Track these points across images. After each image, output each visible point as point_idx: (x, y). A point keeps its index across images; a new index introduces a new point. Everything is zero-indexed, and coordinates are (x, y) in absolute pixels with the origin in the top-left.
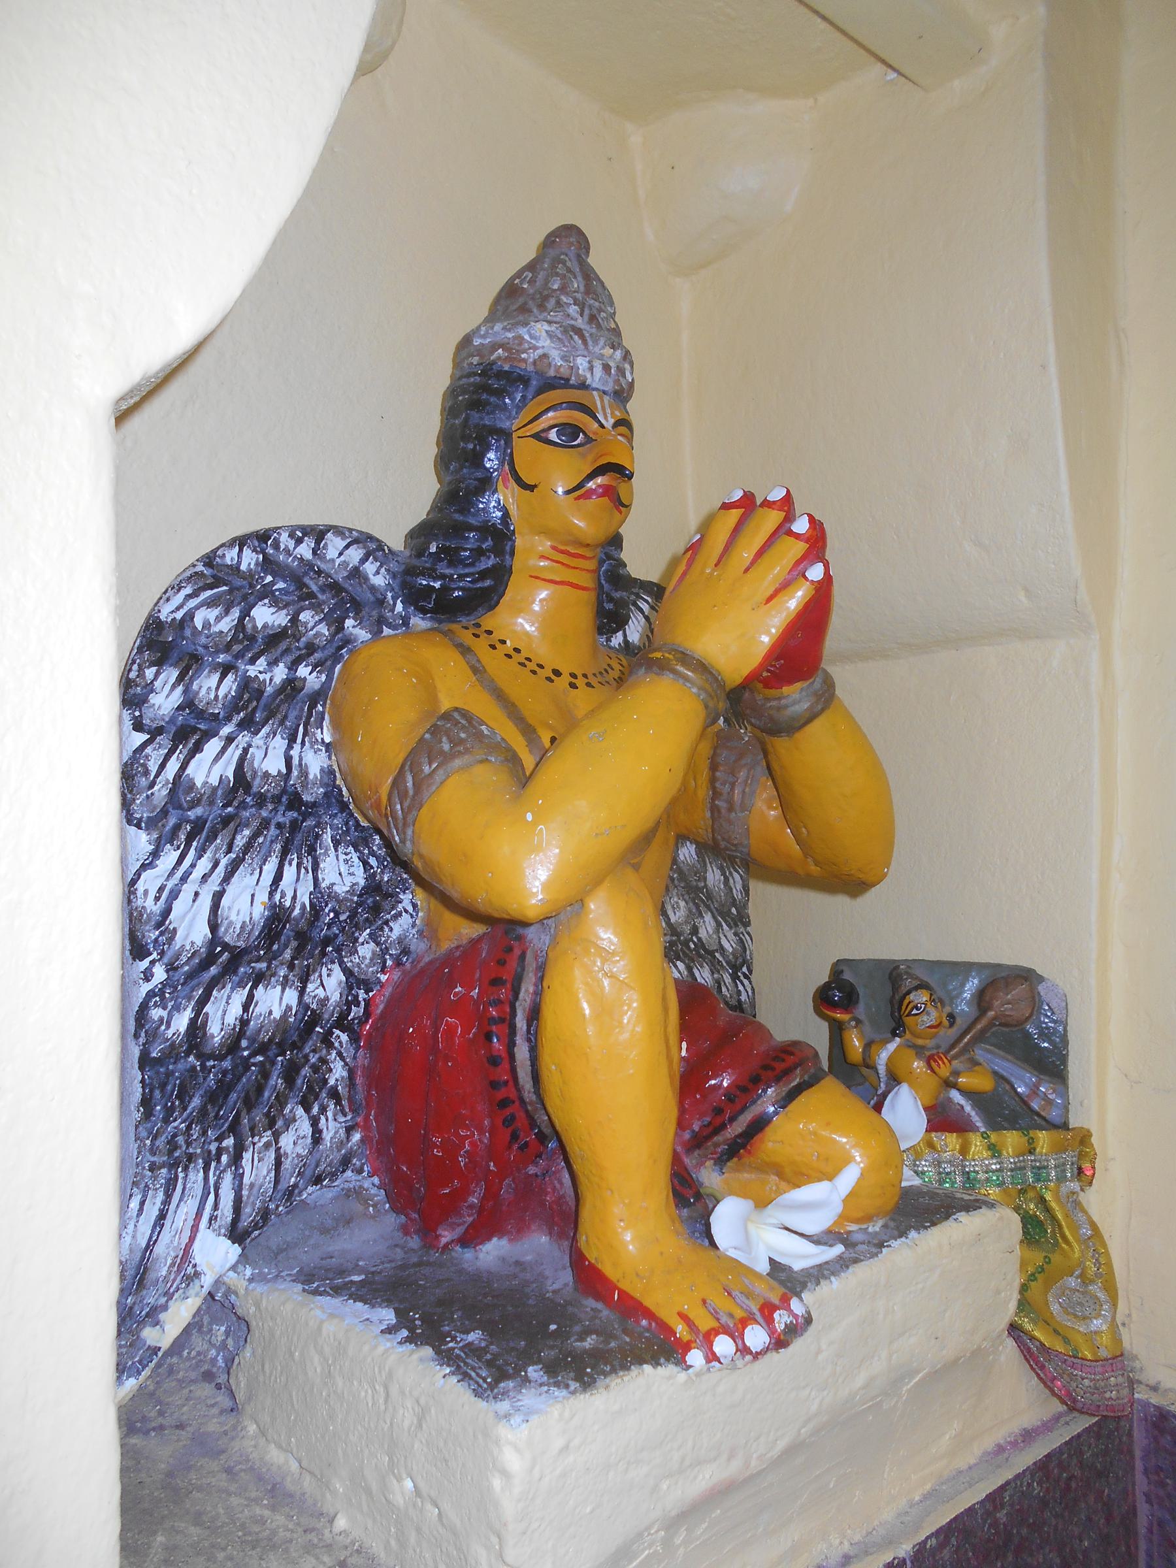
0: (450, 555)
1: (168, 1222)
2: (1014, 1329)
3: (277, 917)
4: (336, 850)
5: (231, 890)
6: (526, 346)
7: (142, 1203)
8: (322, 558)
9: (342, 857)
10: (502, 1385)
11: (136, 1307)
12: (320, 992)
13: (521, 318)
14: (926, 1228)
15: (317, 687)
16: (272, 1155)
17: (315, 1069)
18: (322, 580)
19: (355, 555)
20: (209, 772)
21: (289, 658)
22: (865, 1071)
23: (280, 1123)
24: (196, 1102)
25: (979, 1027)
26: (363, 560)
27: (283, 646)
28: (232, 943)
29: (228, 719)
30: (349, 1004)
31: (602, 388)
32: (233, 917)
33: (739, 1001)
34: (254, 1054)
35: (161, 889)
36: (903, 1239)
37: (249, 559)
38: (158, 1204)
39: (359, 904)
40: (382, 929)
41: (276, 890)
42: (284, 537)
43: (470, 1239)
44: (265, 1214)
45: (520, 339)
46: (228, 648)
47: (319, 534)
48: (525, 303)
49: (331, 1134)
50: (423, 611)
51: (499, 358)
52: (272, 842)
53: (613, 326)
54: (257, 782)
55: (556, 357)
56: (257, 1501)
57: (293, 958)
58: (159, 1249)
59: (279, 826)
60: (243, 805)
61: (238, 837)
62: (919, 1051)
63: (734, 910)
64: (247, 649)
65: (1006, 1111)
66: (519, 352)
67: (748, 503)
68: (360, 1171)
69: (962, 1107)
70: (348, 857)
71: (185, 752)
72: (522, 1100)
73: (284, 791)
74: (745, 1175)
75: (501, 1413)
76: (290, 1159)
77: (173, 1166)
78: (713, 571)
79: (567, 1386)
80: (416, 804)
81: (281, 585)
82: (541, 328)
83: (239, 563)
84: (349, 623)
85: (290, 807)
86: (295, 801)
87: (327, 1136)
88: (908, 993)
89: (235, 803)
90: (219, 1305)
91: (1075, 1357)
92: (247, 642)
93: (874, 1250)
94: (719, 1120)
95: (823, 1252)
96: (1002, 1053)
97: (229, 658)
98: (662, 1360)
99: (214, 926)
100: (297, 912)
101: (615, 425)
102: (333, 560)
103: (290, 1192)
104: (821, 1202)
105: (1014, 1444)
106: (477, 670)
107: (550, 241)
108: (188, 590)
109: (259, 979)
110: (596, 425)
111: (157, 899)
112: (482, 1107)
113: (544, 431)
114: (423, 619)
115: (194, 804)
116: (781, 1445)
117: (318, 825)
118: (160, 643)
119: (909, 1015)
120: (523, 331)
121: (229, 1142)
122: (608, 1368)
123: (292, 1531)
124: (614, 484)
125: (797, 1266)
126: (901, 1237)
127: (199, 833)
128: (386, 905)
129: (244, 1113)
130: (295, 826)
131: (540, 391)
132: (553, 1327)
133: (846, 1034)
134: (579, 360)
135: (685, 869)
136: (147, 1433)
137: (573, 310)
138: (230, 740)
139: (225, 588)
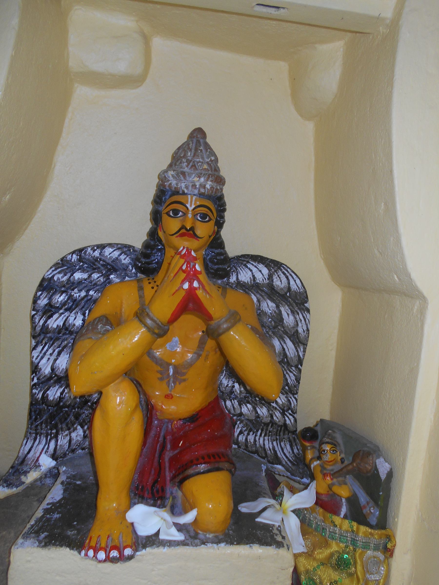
7: (27, 442)
16: (68, 438)
19: (116, 253)
21: (86, 289)
23: (72, 429)
28: (58, 374)
29: (61, 309)
35: (38, 356)
47: (102, 247)
54: (71, 327)
55: (174, 183)
58: (30, 456)
61: (63, 343)
63: (287, 388)
64: (72, 286)
71: (46, 317)
77: (36, 434)
81: (86, 265)
83: (71, 259)
92: (72, 285)
98: (75, 549)
99: (53, 369)
102: (107, 256)
107: (191, 136)
111: (36, 359)
115: (50, 332)
118: (46, 285)
121: (54, 431)
127: (53, 340)
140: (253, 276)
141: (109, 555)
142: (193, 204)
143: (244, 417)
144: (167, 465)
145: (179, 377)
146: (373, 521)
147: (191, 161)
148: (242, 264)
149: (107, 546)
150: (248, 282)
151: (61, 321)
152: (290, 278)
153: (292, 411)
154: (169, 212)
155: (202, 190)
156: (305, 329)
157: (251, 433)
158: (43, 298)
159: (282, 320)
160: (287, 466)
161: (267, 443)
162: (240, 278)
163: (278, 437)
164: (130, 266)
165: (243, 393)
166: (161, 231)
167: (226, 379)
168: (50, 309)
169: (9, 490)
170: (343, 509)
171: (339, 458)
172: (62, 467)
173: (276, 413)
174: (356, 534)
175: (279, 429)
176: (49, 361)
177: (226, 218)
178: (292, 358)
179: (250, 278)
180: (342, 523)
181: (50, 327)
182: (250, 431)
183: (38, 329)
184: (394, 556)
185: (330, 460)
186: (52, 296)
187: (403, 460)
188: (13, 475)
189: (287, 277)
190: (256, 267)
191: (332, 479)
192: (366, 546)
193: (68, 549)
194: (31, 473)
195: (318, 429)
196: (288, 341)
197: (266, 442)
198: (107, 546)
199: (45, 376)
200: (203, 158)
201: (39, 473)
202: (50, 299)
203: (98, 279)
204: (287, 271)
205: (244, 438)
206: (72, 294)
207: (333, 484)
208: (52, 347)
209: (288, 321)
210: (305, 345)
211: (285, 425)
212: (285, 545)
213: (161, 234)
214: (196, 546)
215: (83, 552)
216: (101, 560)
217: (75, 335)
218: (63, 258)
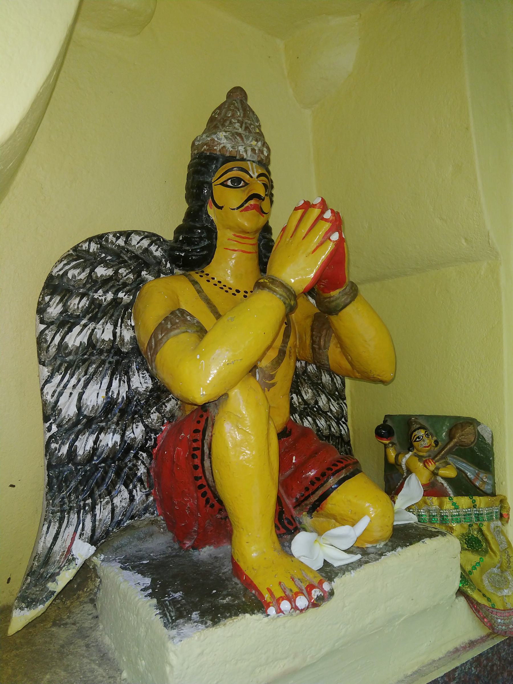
0: (188, 241)
1: (60, 537)
2: (460, 592)
3: (110, 404)
4: (138, 373)
5: (87, 392)
6: (216, 143)
7: (48, 528)
8: (130, 245)
9: (141, 375)
10: (178, 621)
11: (45, 574)
12: (132, 435)
13: (214, 131)
14: (407, 546)
15: (129, 301)
16: (110, 506)
17: (130, 469)
18: (129, 255)
19: (145, 243)
20: (75, 340)
22: (397, 467)
24: (73, 484)
25: (448, 447)
26: (150, 245)
27: (111, 284)
28: (88, 415)
29: (84, 317)
30: (146, 440)
31: (251, 159)
32: (89, 403)
33: (341, 434)
34: (100, 463)
35: (54, 392)
36: (393, 552)
37: (94, 247)
38: (56, 528)
39: (150, 396)
40: (162, 407)
41: (109, 391)
42: (111, 237)
43: (195, 547)
44: (107, 533)
45: (213, 140)
46: (84, 285)
47: (128, 234)
48: (217, 124)
49: (139, 497)
50: (178, 266)
51: (205, 150)
52: (106, 370)
53: (258, 131)
54: (99, 344)
55: (229, 146)
56: (94, 661)
57: (118, 421)
58: (56, 548)
59: (110, 363)
60: (92, 354)
61: (90, 368)
62: (420, 458)
63: (337, 393)
65: (463, 487)
66: (213, 146)
67: (307, 206)
68: (153, 514)
69: (443, 484)
70: (144, 375)
71: (63, 332)
72: (208, 485)
73: (112, 347)
74: (321, 519)
75: (171, 636)
76: (119, 508)
77: (62, 511)
78: (290, 240)
79: (206, 623)
80: (155, 352)
81: (109, 258)
82: (222, 135)
84: (144, 273)
85: (116, 354)
86: (118, 352)
87: (137, 498)
88: (415, 431)
89: (88, 354)
90: (87, 571)
91: (493, 608)
92: (95, 283)
93: (377, 557)
94: (307, 494)
95: (352, 557)
96: (461, 459)
97: (85, 290)
98: (256, 611)
100: (120, 400)
101: (259, 176)
102: (135, 246)
103: (119, 523)
104: (347, 534)
105: (464, 648)
106: (200, 291)
107: (229, 95)
108: (65, 262)
109: (101, 430)
110: (248, 176)
111: (52, 396)
112: (192, 488)
113: (225, 181)
114: (180, 270)
115: (70, 354)
116: (323, 652)
117: (129, 361)
118: (54, 286)
119: (415, 441)
120: (214, 137)
121: (89, 501)
122: (228, 615)
123: (104, 677)
124: (258, 203)
125: (336, 564)
126: (392, 550)
127: (71, 367)
128: (163, 396)
129: (96, 489)
130: (118, 363)
131: (223, 163)
132: (214, 591)
133: (388, 450)
134: (240, 148)
135: (311, 375)
136: (60, 626)
137: (237, 125)
138: (85, 326)
139: (82, 260)
142: (255, 172)
153: (345, 419)
158: (55, 304)
165: (301, 405)
171: (433, 441)
186: (67, 301)
188: (35, 586)
193: (247, 615)
194: (62, 573)
198: (301, 590)
199: (69, 420)
206: (96, 297)
217: (105, 354)
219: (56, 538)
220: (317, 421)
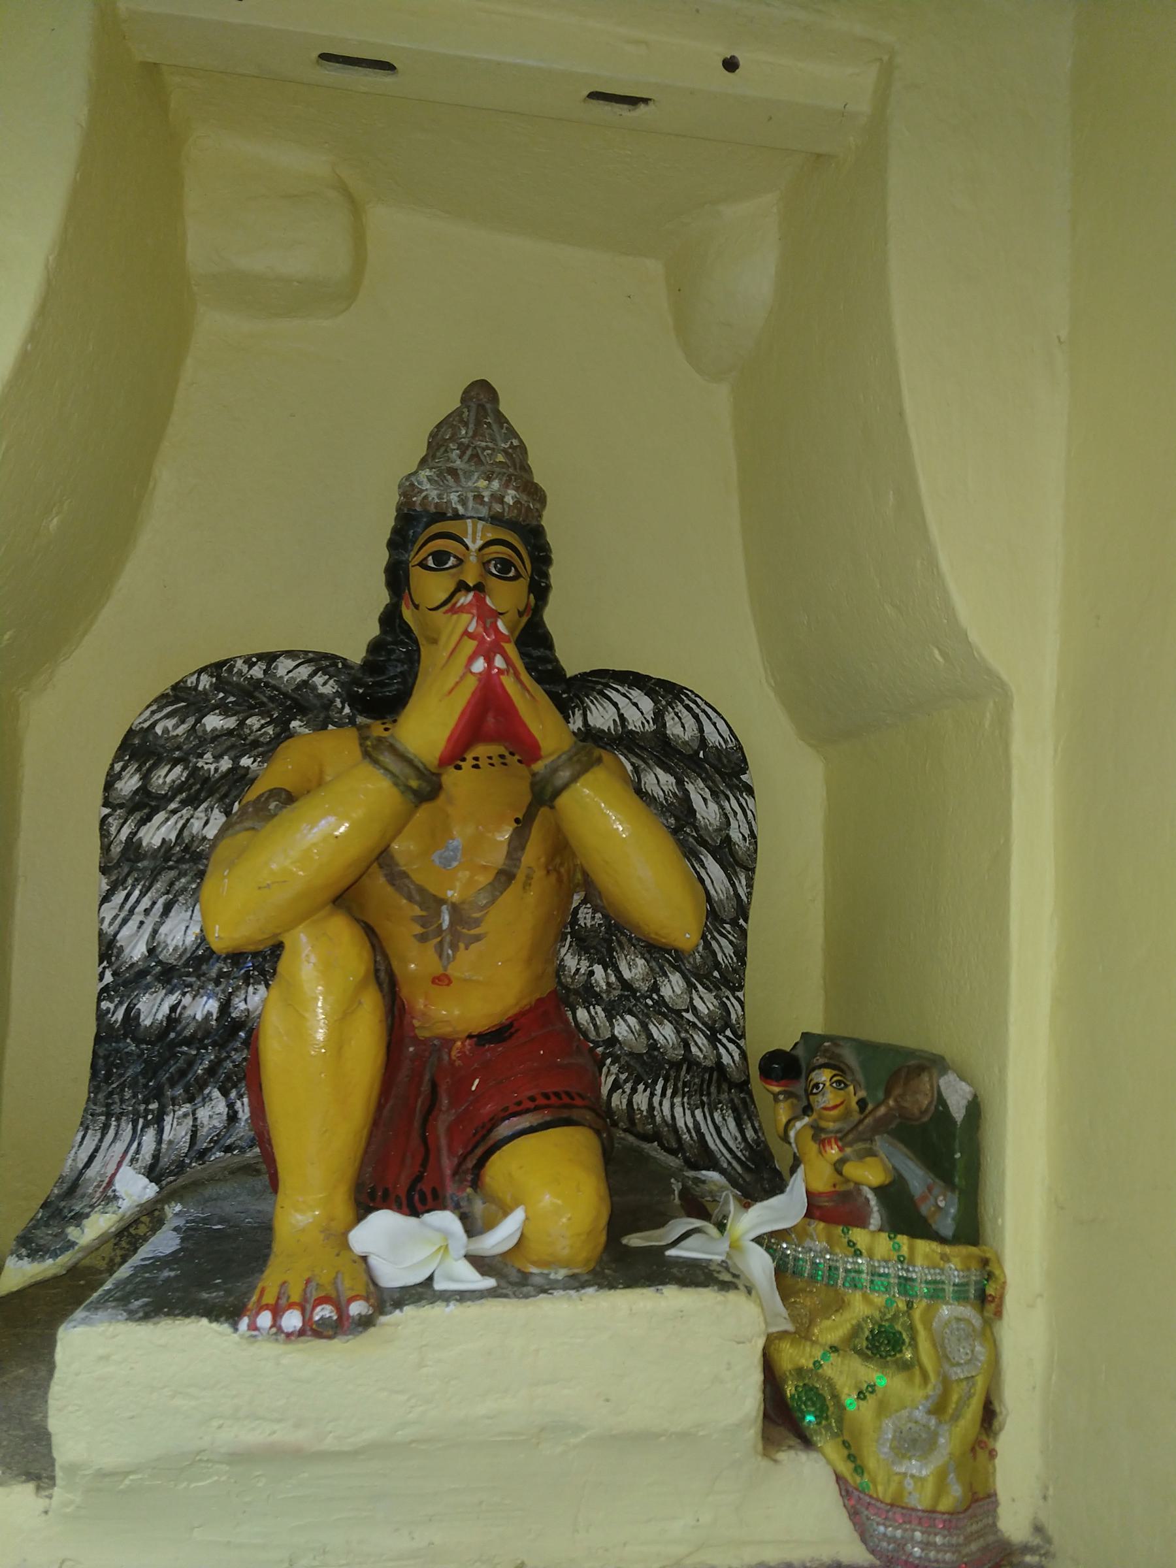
7: (83, 1138)
16: (189, 1121)
19: (304, 672)
23: (199, 1099)
29: (171, 800)
32: (169, 942)
47: (270, 658)
54: (195, 844)
55: (433, 494)
58: (90, 1173)
63: (716, 974)
77: (109, 1115)
81: (232, 699)
83: (197, 685)
99: (151, 951)
102: (281, 677)
107: (466, 397)
111: (111, 924)
118: (138, 748)
129: (166, 1087)
140: (621, 716)
141: (311, 1318)
143: (621, 1048)
144: (443, 1142)
145: (465, 931)
146: (947, 1226)
147: (468, 446)
148: (593, 689)
149: (305, 1300)
150: (609, 729)
151: (170, 831)
152: (703, 717)
154: (425, 559)
155: (498, 508)
156: (747, 833)
157: (641, 1087)
159: (692, 812)
160: (733, 1172)
161: (682, 1115)
162: (591, 722)
163: (705, 1098)
164: (338, 700)
166: (408, 608)
167: (573, 954)
168: (146, 800)
169: (35, 1264)
170: (872, 1221)
171: (854, 1100)
172: (173, 1204)
173: (696, 1037)
174: (909, 1264)
175: (707, 1076)
176: (141, 931)
177: (553, 580)
178: (721, 900)
179: (614, 721)
180: (874, 1242)
181: (144, 844)
182: (636, 1083)
183: (116, 850)
184: (1005, 1312)
185: (832, 1104)
186: (150, 770)
187: (1000, 1071)
188: (47, 1225)
189: (696, 717)
190: (624, 695)
191: (841, 1149)
192: (936, 1293)
194: (93, 1217)
195: (800, 1052)
196: (709, 861)
197: (678, 1111)
198: (305, 1300)
199: (132, 965)
200: (493, 440)
201: (115, 1218)
202: (146, 778)
203: (260, 730)
204: (695, 702)
205: (625, 1101)
206: (199, 765)
207: (843, 1161)
208: (149, 894)
209: (705, 815)
210: (750, 870)
211: (720, 1066)
212: (741, 1287)
213: (407, 614)
214: (527, 1296)
215: (244, 1323)
216: (290, 1330)
218: (178, 683)
219: (92, 1158)
220: (651, 1027)
